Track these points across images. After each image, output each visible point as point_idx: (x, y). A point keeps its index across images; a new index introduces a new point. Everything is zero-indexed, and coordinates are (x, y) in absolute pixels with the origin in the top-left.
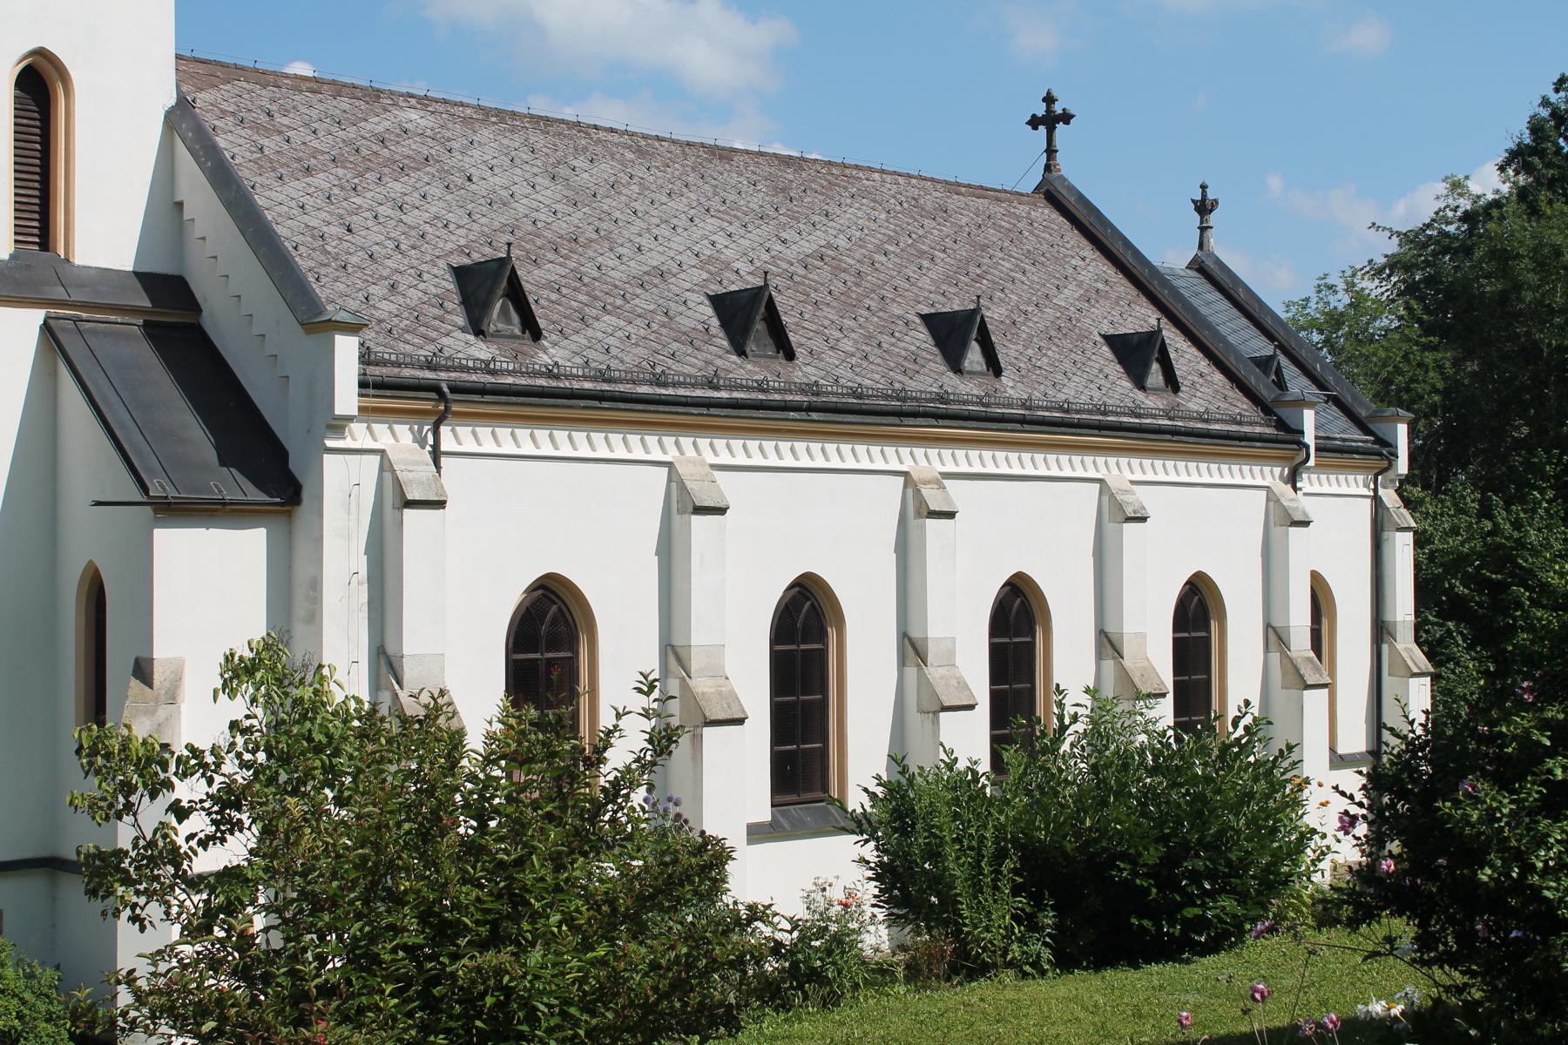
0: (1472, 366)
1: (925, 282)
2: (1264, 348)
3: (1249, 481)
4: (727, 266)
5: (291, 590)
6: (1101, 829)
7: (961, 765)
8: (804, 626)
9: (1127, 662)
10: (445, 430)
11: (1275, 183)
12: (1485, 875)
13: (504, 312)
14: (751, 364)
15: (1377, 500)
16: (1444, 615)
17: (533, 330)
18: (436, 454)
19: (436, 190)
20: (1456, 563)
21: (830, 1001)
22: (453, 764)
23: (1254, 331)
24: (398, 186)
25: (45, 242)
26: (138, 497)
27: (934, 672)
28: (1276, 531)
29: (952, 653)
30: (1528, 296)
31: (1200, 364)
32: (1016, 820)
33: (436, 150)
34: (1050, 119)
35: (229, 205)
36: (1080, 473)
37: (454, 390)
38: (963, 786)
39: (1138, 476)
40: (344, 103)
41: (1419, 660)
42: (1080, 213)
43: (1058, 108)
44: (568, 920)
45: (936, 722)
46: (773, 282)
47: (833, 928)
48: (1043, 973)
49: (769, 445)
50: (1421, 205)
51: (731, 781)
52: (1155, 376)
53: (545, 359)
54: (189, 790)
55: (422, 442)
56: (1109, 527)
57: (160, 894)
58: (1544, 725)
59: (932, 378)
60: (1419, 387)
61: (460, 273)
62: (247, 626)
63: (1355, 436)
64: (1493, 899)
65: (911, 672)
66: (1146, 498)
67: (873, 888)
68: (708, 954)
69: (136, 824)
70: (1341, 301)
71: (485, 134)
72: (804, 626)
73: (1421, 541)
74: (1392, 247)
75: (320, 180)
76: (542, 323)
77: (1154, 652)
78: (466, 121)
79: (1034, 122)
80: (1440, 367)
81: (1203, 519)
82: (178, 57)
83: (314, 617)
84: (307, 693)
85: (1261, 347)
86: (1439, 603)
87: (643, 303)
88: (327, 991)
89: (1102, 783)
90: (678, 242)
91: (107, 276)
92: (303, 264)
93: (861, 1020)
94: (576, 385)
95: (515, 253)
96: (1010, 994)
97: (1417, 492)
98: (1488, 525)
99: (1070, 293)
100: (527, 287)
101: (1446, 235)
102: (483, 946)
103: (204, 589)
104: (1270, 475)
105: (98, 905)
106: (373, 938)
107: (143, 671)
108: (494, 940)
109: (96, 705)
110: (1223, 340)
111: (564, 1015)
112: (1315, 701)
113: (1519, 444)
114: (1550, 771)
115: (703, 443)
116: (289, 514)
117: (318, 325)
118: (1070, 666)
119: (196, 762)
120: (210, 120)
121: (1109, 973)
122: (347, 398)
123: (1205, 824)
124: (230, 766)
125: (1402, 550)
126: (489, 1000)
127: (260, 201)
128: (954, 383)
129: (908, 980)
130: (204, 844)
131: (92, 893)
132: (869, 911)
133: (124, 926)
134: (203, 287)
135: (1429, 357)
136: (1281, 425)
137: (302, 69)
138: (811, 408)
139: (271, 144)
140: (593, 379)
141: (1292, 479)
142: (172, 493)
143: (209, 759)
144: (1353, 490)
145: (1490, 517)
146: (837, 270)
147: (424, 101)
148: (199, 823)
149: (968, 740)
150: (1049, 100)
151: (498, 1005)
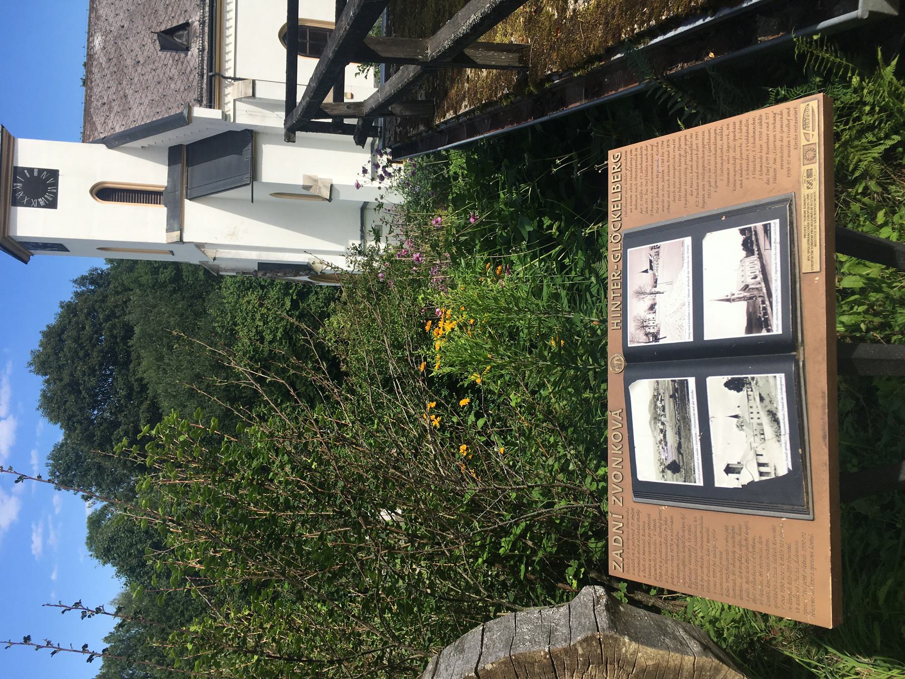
13: (180, 37)
17: (186, 26)
26: (250, 186)
29: (310, 178)
75: (130, 92)
82: (83, 142)
94: (207, 14)
122: (215, 114)
142: (248, 175)
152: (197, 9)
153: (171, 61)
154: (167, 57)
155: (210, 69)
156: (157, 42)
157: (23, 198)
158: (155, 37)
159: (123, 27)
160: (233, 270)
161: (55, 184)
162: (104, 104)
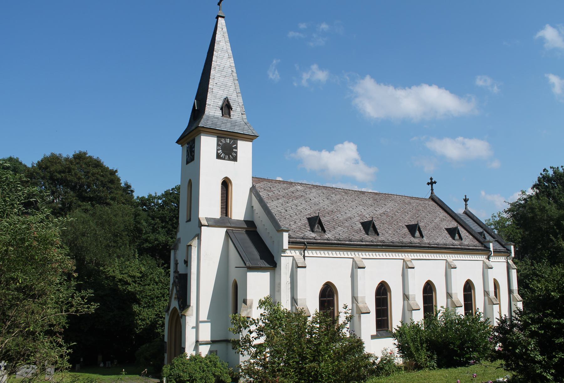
0: (527, 233)
1: (406, 218)
2: (480, 230)
3: (479, 259)
4: (364, 216)
5: (275, 286)
6: (447, 337)
7: (415, 323)
8: (383, 292)
9: (453, 299)
10: (306, 252)
11: (483, 193)
12: (517, 351)
13: (318, 227)
14: (369, 237)
15: (507, 262)
16: (524, 288)
18: (304, 257)
19: (304, 202)
20: (527, 276)
21: (388, 374)
22: (305, 323)
23: (478, 226)
24: (296, 202)
25: (227, 215)
27: (411, 302)
28: (485, 270)
30: (538, 217)
31: (467, 234)
32: (428, 335)
33: (304, 194)
34: (432, 183)
35: (262, 206)
36: (441, 258)
37: (308, 243)
38: (416, 328)
39: (454, 259)
40: (285, 185)
41: (520, 298)
42: (439, 203)
43: (433, 181)
44: (329, 356)
45: (412, 313)
46: (374, 219)
47: (388, 358)
48: (435, 369)
49: (374, 254)
50: (516, 197)
51: (368, 325)
52: (457, 237)
53: (326, 236)
54: (253, 328)
55: (301, 254)
56: (448, 270)
57: (247, 349)
58: (530, 318)
59: (409, 239)
60: (516, 238)
61: (309, 219)
62: (265, 293)
63: (502, 249)
64: (520, 356)
65: (406, 302)
66: (456, 263)
67: (397, 350)
68: (359, 364)
69: (242, 334)
70: (497, 219)
71: (313, 190)
72: (383, 292)
73: (518, 271)
74: (509, 207)
75: (280, 201)
76: (326, 229)
77: (460, 297)
78: (310, 188)
79: (428, 184)
80: (520, 233)
81: (469, 268)
83: (279, 291)
84: (276, 308)
85: (480, 230)
86: (523, 285)
87: (347, 224)
88: (279, 370)
89: (447, 327)
90: (354, 211)
91: (238, 221)
92: (277, 218)
93: (395, 379)
95: (320, 214)
96: (427, 374)
97: (517, 260)
98: (533, 268)
99: (438, 219)
100: (323, 222)
101: (521, 204)
102: (311, 362)
103: (257, 285)
104: (483, 258)
105: (234, 351)
106: (289, 360)
107: (245, 302)
108: (314, 360)
109: (236, 310)
110: (471, 228)
111: (329, 377)
112: (496, 307)
113: (539, 249)
114: (531, 328)
115: (360, 253)
116: (274, 270)
117: (280, 230)
118: (441, 301)
119: (254, 322)
120: (259, 189)
121: (450, 369)
122: (286, 245)
123: (470, 336)
124: (261, 323)
125: (514, 273)
126: (313, 373)
127: (268, 205)
128: (413, 239)
129: (405, 370)
130: (255, 339)
131: (233, 348)
132: (396, 354)
133: (241, 356)
134: (257, 223)
135: (517, 231)
136: (485, 247)
137: (281, 179)
138: (383, 246)
139: (270, 194)
140: (337, 240)
141: (488, 258)
143: (256, 321)
144: (502, 260)
145: (533, 266)
146: (388, 216)
147: (301, 184)
148: (254, 335)
149: (418, 317)
150: (431, 179)
151: (315, 374)
161: (229, 159)
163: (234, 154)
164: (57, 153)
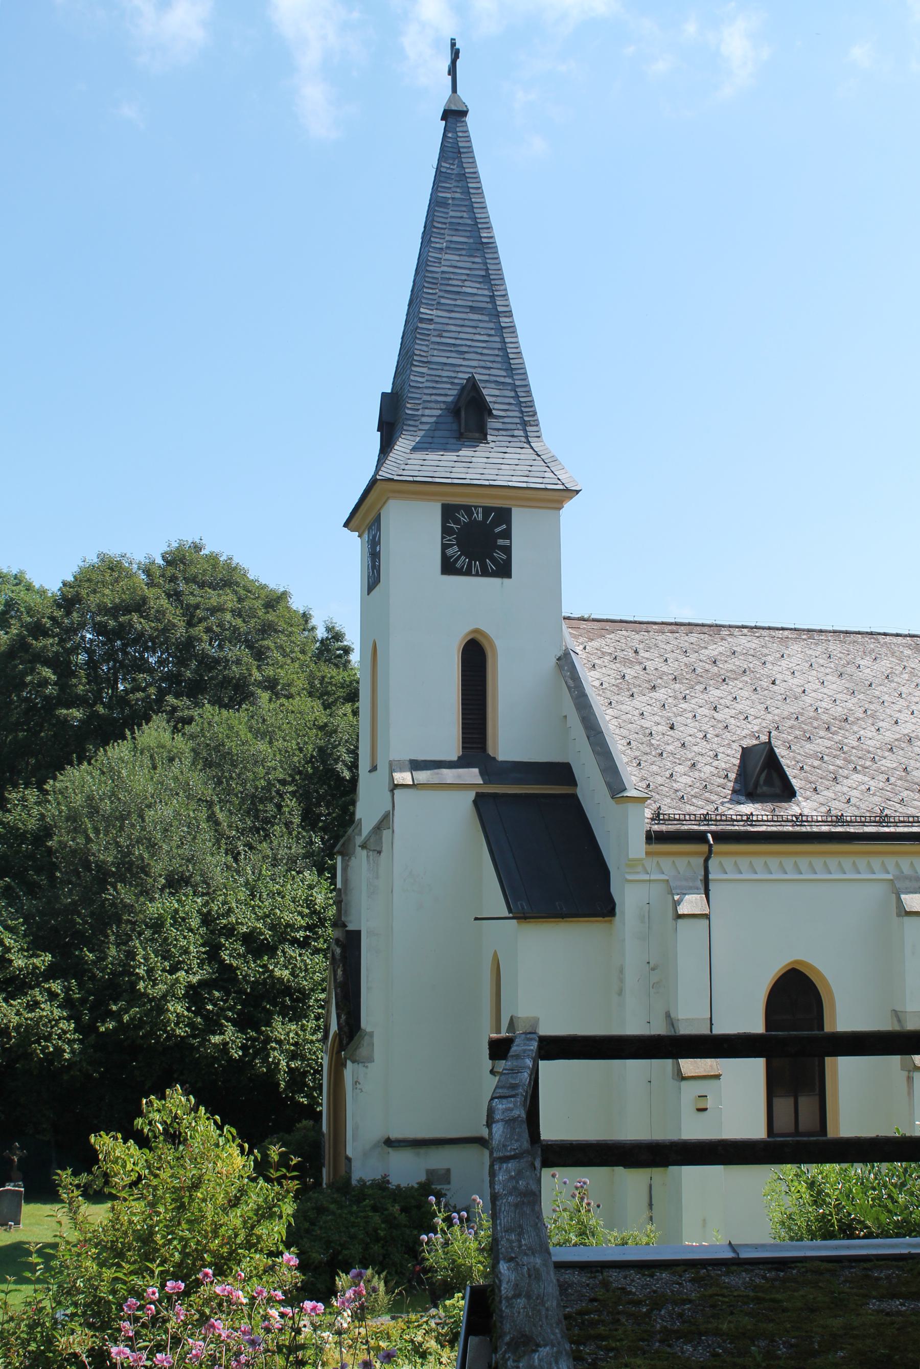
17: (788, 793)
24: (717, 693)
26: (506, 914)
40: (693, 638)
87: (889, 762)
152: (824, 809)
153: (723, 766)
154: (731, 760)
155: (721, 837)
156: (755, 742)
157: (457, 521)
158: (764, 738)
159: (774, 683)
160: (345, 881)
161: (485, 573)
162: (636, 652)
163: (500, 555)
164: (114, 550)
